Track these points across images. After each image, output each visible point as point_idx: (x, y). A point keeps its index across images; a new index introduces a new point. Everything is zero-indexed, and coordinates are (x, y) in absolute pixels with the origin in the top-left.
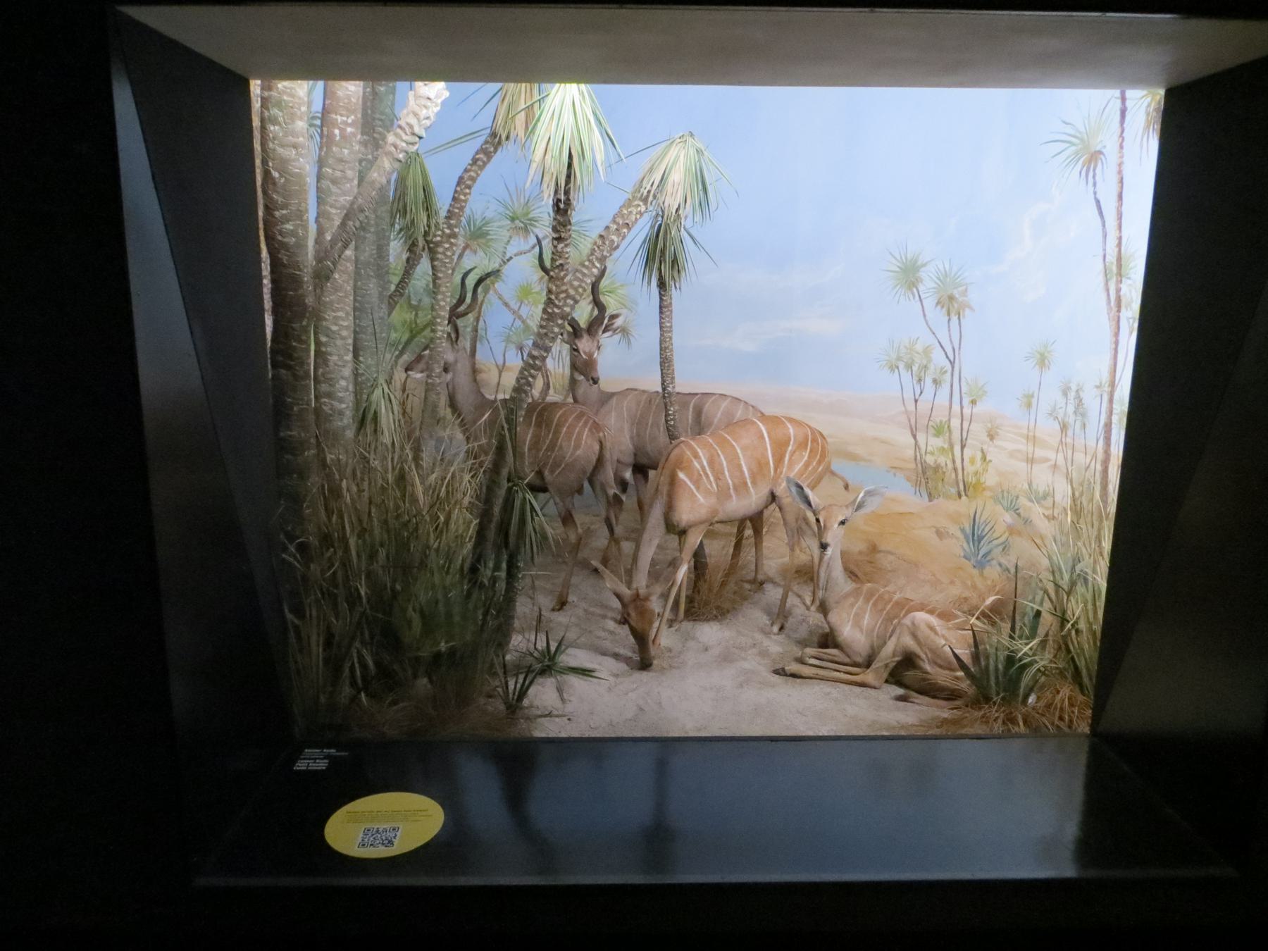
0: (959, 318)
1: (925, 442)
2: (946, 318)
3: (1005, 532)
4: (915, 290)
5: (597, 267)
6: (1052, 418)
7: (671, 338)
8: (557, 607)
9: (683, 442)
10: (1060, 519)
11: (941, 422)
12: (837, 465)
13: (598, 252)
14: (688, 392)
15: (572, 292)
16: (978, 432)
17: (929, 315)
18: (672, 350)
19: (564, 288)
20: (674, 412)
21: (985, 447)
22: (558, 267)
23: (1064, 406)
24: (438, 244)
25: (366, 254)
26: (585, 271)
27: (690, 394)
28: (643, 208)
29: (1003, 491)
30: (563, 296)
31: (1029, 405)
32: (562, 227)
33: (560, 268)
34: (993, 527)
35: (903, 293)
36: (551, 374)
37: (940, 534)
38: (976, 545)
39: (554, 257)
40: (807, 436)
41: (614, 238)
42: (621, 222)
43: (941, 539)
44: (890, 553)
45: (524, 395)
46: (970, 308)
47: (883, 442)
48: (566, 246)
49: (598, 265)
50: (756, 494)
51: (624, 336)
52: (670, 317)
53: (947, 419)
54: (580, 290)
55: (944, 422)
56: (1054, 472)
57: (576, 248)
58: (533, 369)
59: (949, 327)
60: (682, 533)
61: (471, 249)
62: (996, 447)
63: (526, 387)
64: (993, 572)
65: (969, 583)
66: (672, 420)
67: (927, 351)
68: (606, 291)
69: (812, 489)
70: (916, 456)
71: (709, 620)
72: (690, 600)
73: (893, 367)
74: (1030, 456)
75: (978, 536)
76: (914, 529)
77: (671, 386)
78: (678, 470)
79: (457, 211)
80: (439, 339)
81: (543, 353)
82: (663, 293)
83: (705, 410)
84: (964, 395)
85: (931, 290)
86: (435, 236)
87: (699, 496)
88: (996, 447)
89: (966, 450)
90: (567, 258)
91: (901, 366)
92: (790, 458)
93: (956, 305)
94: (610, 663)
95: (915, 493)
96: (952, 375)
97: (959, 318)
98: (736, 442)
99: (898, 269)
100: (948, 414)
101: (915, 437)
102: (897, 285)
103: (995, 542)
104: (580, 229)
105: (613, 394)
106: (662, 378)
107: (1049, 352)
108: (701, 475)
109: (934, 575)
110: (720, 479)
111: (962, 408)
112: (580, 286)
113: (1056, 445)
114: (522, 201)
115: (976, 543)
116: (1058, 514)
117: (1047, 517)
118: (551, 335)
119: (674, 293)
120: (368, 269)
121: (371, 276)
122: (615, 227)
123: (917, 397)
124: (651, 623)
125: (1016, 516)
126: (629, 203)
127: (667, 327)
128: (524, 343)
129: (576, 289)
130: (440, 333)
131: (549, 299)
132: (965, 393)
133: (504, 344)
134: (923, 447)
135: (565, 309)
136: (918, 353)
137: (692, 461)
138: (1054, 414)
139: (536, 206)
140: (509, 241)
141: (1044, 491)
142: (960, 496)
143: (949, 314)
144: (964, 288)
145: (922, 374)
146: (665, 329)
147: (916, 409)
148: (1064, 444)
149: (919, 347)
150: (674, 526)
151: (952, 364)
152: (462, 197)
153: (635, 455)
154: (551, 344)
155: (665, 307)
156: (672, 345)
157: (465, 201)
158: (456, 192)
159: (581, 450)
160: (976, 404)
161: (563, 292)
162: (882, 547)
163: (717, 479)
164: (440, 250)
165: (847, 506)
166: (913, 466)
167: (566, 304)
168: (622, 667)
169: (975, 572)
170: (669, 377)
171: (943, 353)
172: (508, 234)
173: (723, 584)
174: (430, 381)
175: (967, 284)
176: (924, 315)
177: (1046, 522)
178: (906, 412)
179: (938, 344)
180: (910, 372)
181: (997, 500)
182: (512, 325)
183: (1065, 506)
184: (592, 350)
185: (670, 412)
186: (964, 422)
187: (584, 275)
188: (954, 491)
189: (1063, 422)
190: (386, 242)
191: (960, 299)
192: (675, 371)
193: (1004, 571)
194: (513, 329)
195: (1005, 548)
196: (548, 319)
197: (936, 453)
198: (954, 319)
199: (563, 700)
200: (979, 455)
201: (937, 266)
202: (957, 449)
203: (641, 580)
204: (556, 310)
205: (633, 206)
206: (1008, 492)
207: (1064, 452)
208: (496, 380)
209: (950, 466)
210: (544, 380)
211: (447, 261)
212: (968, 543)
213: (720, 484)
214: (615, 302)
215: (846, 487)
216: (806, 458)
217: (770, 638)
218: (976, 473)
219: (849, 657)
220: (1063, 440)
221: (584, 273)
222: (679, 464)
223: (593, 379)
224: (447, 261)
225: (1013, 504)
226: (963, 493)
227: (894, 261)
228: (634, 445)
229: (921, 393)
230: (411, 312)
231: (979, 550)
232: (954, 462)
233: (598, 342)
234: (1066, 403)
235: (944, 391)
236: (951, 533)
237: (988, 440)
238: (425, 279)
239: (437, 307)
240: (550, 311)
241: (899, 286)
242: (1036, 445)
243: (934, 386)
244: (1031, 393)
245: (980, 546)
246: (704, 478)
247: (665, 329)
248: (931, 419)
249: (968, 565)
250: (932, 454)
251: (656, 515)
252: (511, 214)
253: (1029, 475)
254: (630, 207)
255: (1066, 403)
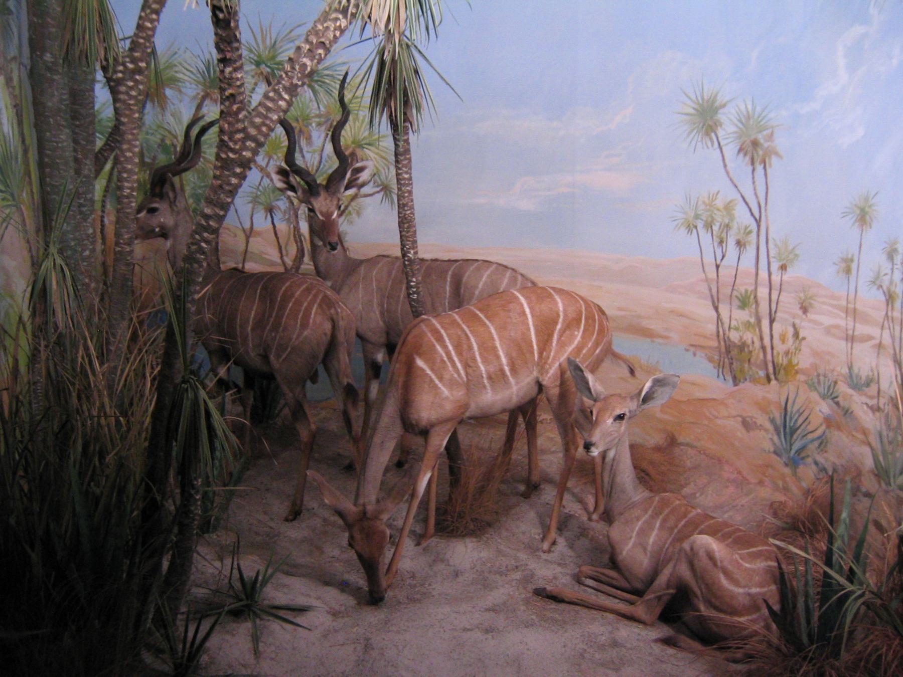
0: (765, 168)
1: (729, 316)
2: (750, 168)
3: (821, 425)
4: (713, 135)
5: (285, 99)
6: (876, 287)
7: (410, 192)
8: (290, 517)
9: (423, 321)
10: (886, 411)
11: (746, 291)
12: (623, 344)
13: (286, 79)
14: (447, 259)
15: (253, 131)
16: (788, 302)
17: (730, 165)
18: (412, 208)
19: (240, 126)
20: (417, 284)
21: (797, 321)
22: (228, 98)
23: (889, 272)
24: (119, 82)
25: (55, 100)
26: (270, 105)
27: (449, 261)
28: (343, 23)
29: (818, 375)
30: (239, 136)
31: (848, 271)
32: (226, 44)
33: (232, 100)
34: (807, 418)
35: (699, 139)
36: (305, 238)
37: (747, 425)
38: (788, 439)
39: (222, 85)
40: (581, 312)
41: (306, 61)
42: (314, 41)
43: (748, 431)
44: (688, 445)
45: (196, 265)
46: (777, 154)
47: (681, 315)
48: (236, 70)
49: (286, 97)
50: (517, 383)
51: (387, 195)
52: (409, 166)
53: (753, 288)
54: (264, 129)
55: (749, 292)
56: (878, 354)
57: (331, 95)
58: (207, 231)
59: (753, 178)
60: (425, 433)
61: (211, 99)
62: (810, 321)
63: (198, 255)
64: (808, 472)
65: (780, 483)
66: (414, 293)
67: (729, 208)
68: (366, 144)
69: (592, 371)
70: (718, 332)
71: (464, 536)
72: (441, 512)
73: (691, 227)
74: (850, 332)
75: (791, 428)
76: (717, 418)
77: (412, 252)
78: (415, 356)
79: (141, 41)
80: (127, 197)
81: (217, 211)
82: (397, 137)
83: (465, 279)
84: (772, 260)
85: (731, 135)
86: (115, 72)
87: (443, 388)
88: (810, 321)
89: (775, 325)
90: (239, 87)
91: (700, 224)
92: (559, 339)
93: (761, 153)
94: (332, 595)
95: (718, 376)
96: (758, 236)
97: (765, 168)
98: (490, 321)
99: (693, 111)
100: (753, 282)
101: (716, 309)
102: (692, 131)
103: (810, 436)
104: (334, 73)
105: (362, 262)
106: (401, 242)
107: (870, 206)
108: (444, 362)
109: (739, 473)
110: (470, 366)
111: (770, 274)
112: (263, 124)
113: (882, 320)
114: (268, 43)
115: (788, 437)
116: (884, 405)
117: (871, 408)
118: (227, 188)
119: (412, 138)
120: (59, 118)
121: (63, 126)
122: (308, 47)
123: (718, 262)
124: (381, 549)
125: (834, 405)
126: (325, 17)
127: (405, 179)
128: (274, 204)
129: (258, 128)
130: (128, 191)
131: (222, 141)
132: (774, 257)
133: (250, 205)
134: (726, 320)
135: (244, 153)
136: (718, 210)
137: (434, 346)
138: (878, 282)
139: (284, 48)
140: (254, 89)
141: (867, 377)
142: (769, 380)
143: (753, 163)
144: (769, 132)
145: (724, 235)
146: (403, 182)
147: (718, 276)
148: (890, 318)
149: (719, 203)
150: (412, 425)
151: (758, 222)
152: (149, 25)
153: (388, 334)
154: (229, 200)
155: (401, 155)
156: (412, 201)
157: (154, 29)
158: (140, 18)
159: (309, 330)
160: (786, 269)
161: (239, 131)
162: (681, 439)
163: (466, 366)
164: (123, 89)
165: (632, 398)
166: (716, 344)
167: (245, 148)
168: (349, 601)
169: (787, 471)
170: (409, 241)
171: (748, 210)
172: (253, 81)
173: (481, 490)
174: (118, 249)
175: (772, 127)
176: (725, 166)
177: (871, 414)
178: (707, 280)
179: (741, 199)
180: (709, 234)
181: (812, 387)
182: (260, 184)
183: (893, 395)
184: (331, 210)
185: (412, 284)
186: (773, 291)
187: (268, 109)
188: (762, 373)
189: (889, 291)
190: (88, 87)
191: (766, 145)
192: (418, 233)
193: (821, 471)
194: (260, 188)
195: (823, 443)
196: (222, 167)
197: (741, 328)
198: (759, 168)
199: (256, 652)
200: (791, 331)
201: (737, 106)
202: (765, 323)
203: (371, 493)
204: (231, 155)
205: (330, 20)
206: (825, 376)
207: (890, 329)
208: (242, 247)
209: (757, 344)
210: (297, 246)
211: (132, 102)
212: (780, 438)
213: (470, 371)
214: (376, 156)
215: (632, 372)
216: (579, 338)
217: (539, 558)
218: (787, 353)
219: (628, 582)
220: (890, 313)
221: (269, 107)
222: (418, 349)
223: (330, 244)
224: (132, 102)
225: (831, 391)
226: (772, 377)
227: (689, 102)
228: (384, 322)
229: (723, 257)
230: (145, 172)
231: (791, 445)
232: (761, 339)
233: (339, 200)
234: (892, 269)
235: (750, 252)
236: (758, 424)
237: (800, 312)
238: (160, 133)
239: (122, 159)
240: (223, 156)
241: (695, 131)
242: (857, 320)
243: (738, 249)
244: (850, 256)
245: (793, 440)
246: (449, 364)
247: (403, 182)
248: (736, 288)
249: (778, 462)
250: (737, 329)
251: (391, 408)
252: (255, 58)
253: (849, 356)
254: (325, 21)
255: (892, 269)
